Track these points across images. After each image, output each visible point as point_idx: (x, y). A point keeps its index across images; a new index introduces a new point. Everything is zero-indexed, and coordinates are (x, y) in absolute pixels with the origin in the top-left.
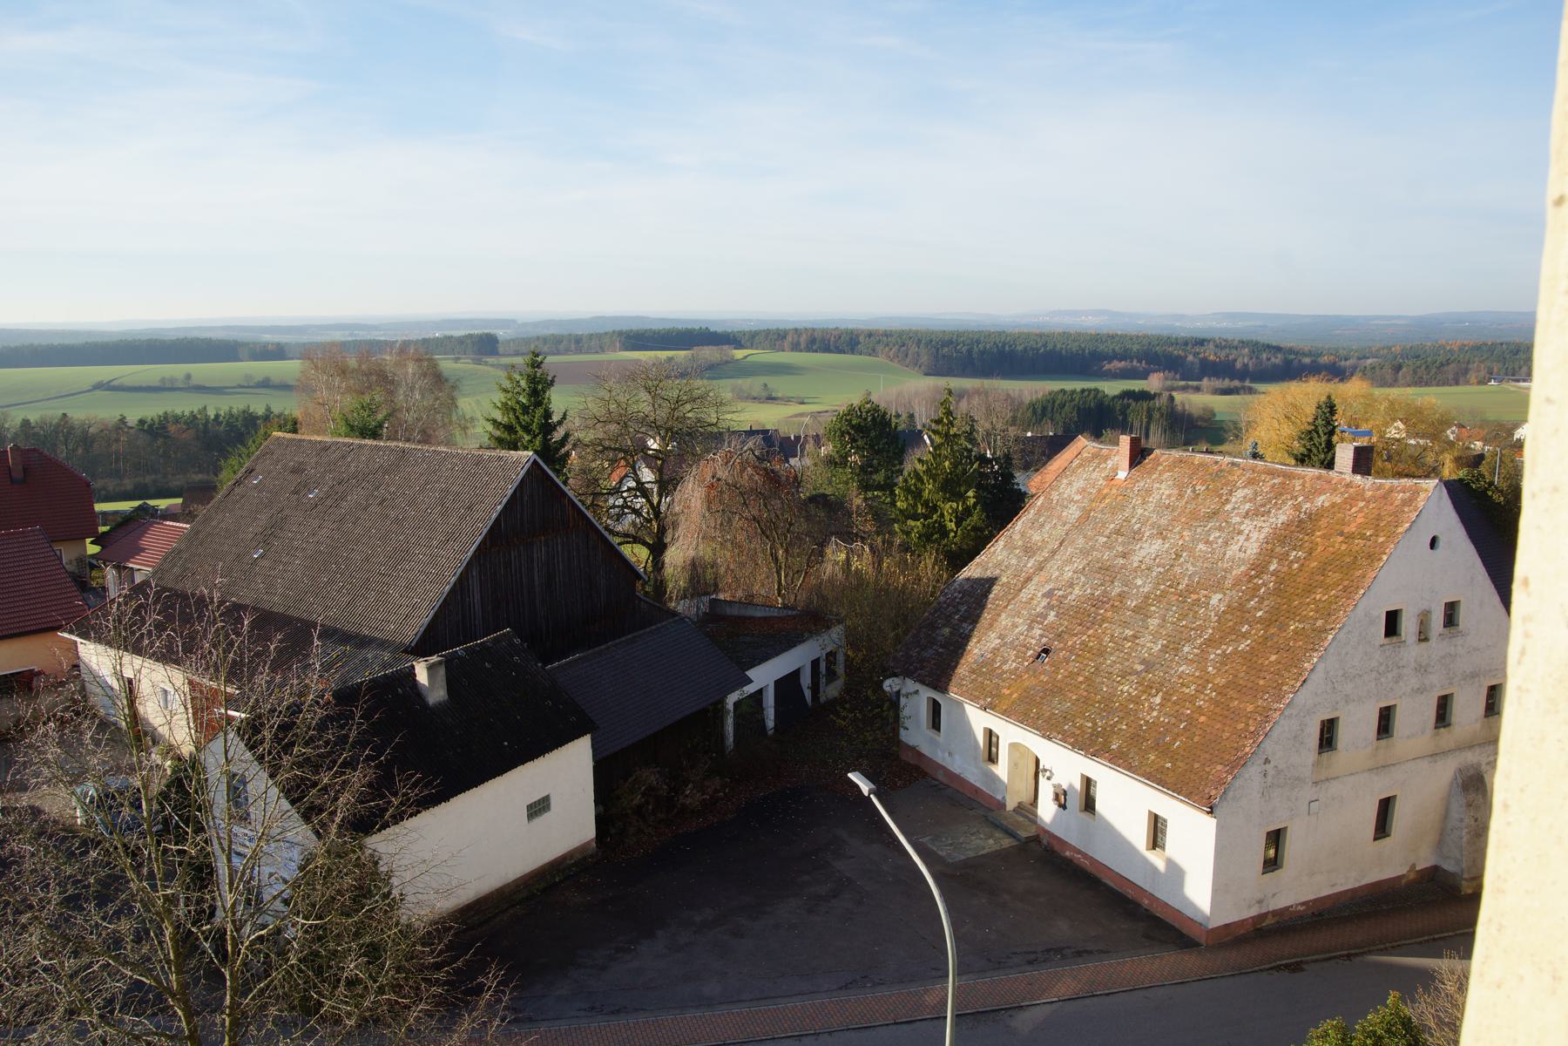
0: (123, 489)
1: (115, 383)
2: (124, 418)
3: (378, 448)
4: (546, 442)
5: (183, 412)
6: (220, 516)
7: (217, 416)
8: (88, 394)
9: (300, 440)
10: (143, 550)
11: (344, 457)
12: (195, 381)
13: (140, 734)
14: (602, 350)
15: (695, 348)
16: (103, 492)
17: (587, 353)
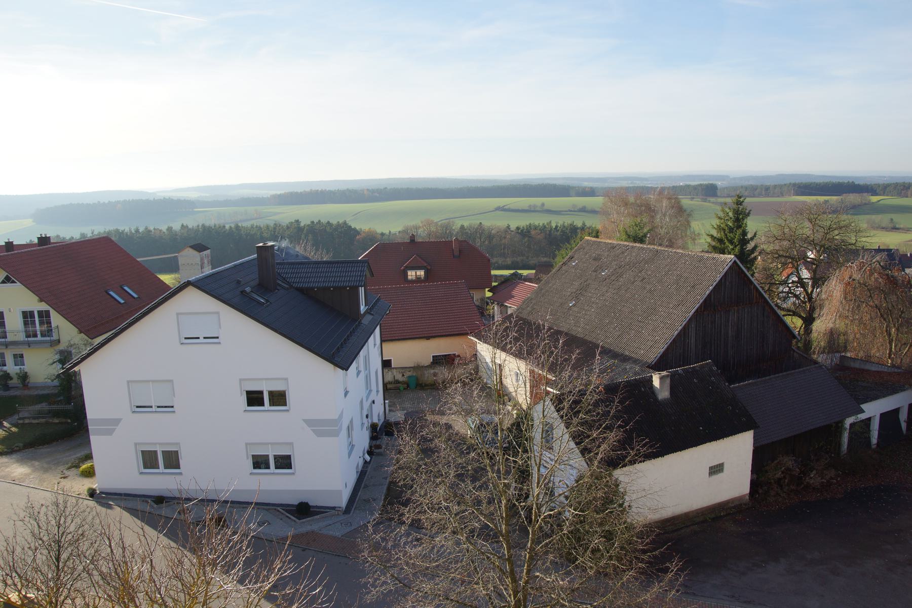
2: (509, 226)
7: (557, 227)
11: (623, 253)
12: (546, 207)
15: (844, 195)
17: (772, 197)
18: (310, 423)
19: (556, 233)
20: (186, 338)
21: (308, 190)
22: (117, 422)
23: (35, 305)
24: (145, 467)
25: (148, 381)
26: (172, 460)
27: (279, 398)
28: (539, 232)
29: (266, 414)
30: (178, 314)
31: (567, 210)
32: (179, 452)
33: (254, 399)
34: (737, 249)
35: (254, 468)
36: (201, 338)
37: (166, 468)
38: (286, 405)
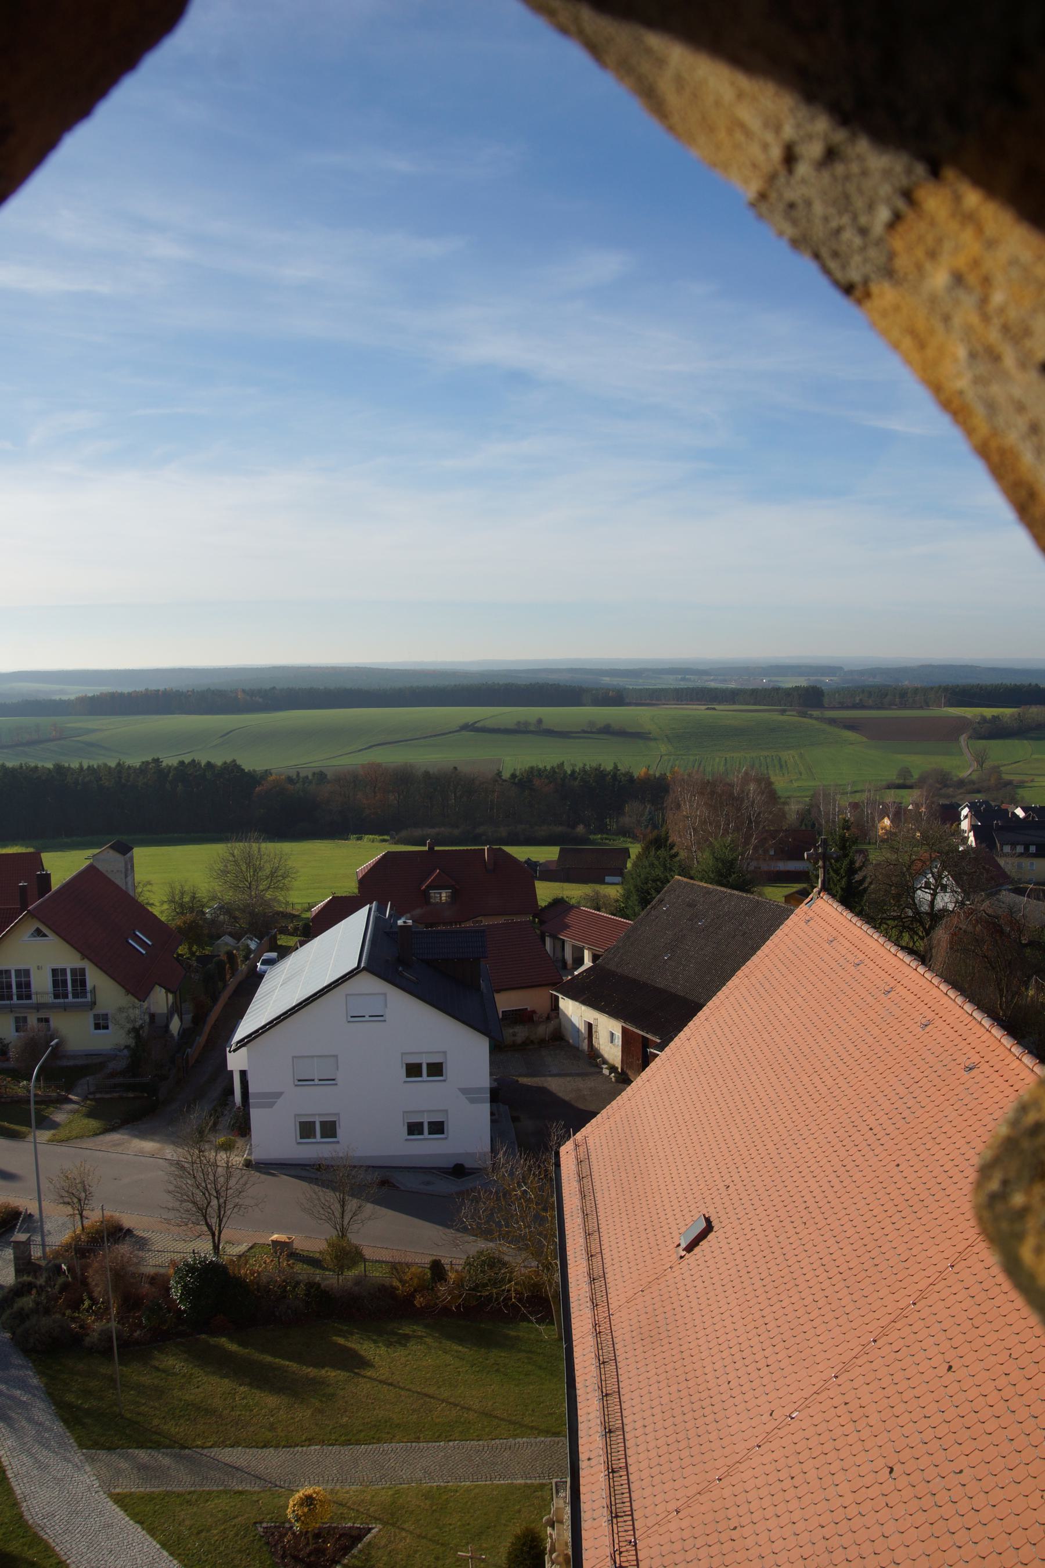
2: (501, 772)
3: (742, 898)
4: (849, 882)
5: (545, 767)
7: (573, 772)
8: (456, 734)
10: (569, 927)
11: (720, 900)
13: (594, 1056)
14: (927, 705)
15: (1023, 707)
16: (484, 838)
17: (911, 708)
20: (352, 1017)
21: (140, 688)
22: (278, 1095)
23: (68, 959)
25: (313, 1057)
26: (330, 1129)
27: (436, 1070)
30: (347, 995)
31: (579, 730)
32: (337, 1123)
33: (413, 1070)
34: (844, 882)
35: (409, 1134)
36: (367, 1017)
37: (322, 1137)
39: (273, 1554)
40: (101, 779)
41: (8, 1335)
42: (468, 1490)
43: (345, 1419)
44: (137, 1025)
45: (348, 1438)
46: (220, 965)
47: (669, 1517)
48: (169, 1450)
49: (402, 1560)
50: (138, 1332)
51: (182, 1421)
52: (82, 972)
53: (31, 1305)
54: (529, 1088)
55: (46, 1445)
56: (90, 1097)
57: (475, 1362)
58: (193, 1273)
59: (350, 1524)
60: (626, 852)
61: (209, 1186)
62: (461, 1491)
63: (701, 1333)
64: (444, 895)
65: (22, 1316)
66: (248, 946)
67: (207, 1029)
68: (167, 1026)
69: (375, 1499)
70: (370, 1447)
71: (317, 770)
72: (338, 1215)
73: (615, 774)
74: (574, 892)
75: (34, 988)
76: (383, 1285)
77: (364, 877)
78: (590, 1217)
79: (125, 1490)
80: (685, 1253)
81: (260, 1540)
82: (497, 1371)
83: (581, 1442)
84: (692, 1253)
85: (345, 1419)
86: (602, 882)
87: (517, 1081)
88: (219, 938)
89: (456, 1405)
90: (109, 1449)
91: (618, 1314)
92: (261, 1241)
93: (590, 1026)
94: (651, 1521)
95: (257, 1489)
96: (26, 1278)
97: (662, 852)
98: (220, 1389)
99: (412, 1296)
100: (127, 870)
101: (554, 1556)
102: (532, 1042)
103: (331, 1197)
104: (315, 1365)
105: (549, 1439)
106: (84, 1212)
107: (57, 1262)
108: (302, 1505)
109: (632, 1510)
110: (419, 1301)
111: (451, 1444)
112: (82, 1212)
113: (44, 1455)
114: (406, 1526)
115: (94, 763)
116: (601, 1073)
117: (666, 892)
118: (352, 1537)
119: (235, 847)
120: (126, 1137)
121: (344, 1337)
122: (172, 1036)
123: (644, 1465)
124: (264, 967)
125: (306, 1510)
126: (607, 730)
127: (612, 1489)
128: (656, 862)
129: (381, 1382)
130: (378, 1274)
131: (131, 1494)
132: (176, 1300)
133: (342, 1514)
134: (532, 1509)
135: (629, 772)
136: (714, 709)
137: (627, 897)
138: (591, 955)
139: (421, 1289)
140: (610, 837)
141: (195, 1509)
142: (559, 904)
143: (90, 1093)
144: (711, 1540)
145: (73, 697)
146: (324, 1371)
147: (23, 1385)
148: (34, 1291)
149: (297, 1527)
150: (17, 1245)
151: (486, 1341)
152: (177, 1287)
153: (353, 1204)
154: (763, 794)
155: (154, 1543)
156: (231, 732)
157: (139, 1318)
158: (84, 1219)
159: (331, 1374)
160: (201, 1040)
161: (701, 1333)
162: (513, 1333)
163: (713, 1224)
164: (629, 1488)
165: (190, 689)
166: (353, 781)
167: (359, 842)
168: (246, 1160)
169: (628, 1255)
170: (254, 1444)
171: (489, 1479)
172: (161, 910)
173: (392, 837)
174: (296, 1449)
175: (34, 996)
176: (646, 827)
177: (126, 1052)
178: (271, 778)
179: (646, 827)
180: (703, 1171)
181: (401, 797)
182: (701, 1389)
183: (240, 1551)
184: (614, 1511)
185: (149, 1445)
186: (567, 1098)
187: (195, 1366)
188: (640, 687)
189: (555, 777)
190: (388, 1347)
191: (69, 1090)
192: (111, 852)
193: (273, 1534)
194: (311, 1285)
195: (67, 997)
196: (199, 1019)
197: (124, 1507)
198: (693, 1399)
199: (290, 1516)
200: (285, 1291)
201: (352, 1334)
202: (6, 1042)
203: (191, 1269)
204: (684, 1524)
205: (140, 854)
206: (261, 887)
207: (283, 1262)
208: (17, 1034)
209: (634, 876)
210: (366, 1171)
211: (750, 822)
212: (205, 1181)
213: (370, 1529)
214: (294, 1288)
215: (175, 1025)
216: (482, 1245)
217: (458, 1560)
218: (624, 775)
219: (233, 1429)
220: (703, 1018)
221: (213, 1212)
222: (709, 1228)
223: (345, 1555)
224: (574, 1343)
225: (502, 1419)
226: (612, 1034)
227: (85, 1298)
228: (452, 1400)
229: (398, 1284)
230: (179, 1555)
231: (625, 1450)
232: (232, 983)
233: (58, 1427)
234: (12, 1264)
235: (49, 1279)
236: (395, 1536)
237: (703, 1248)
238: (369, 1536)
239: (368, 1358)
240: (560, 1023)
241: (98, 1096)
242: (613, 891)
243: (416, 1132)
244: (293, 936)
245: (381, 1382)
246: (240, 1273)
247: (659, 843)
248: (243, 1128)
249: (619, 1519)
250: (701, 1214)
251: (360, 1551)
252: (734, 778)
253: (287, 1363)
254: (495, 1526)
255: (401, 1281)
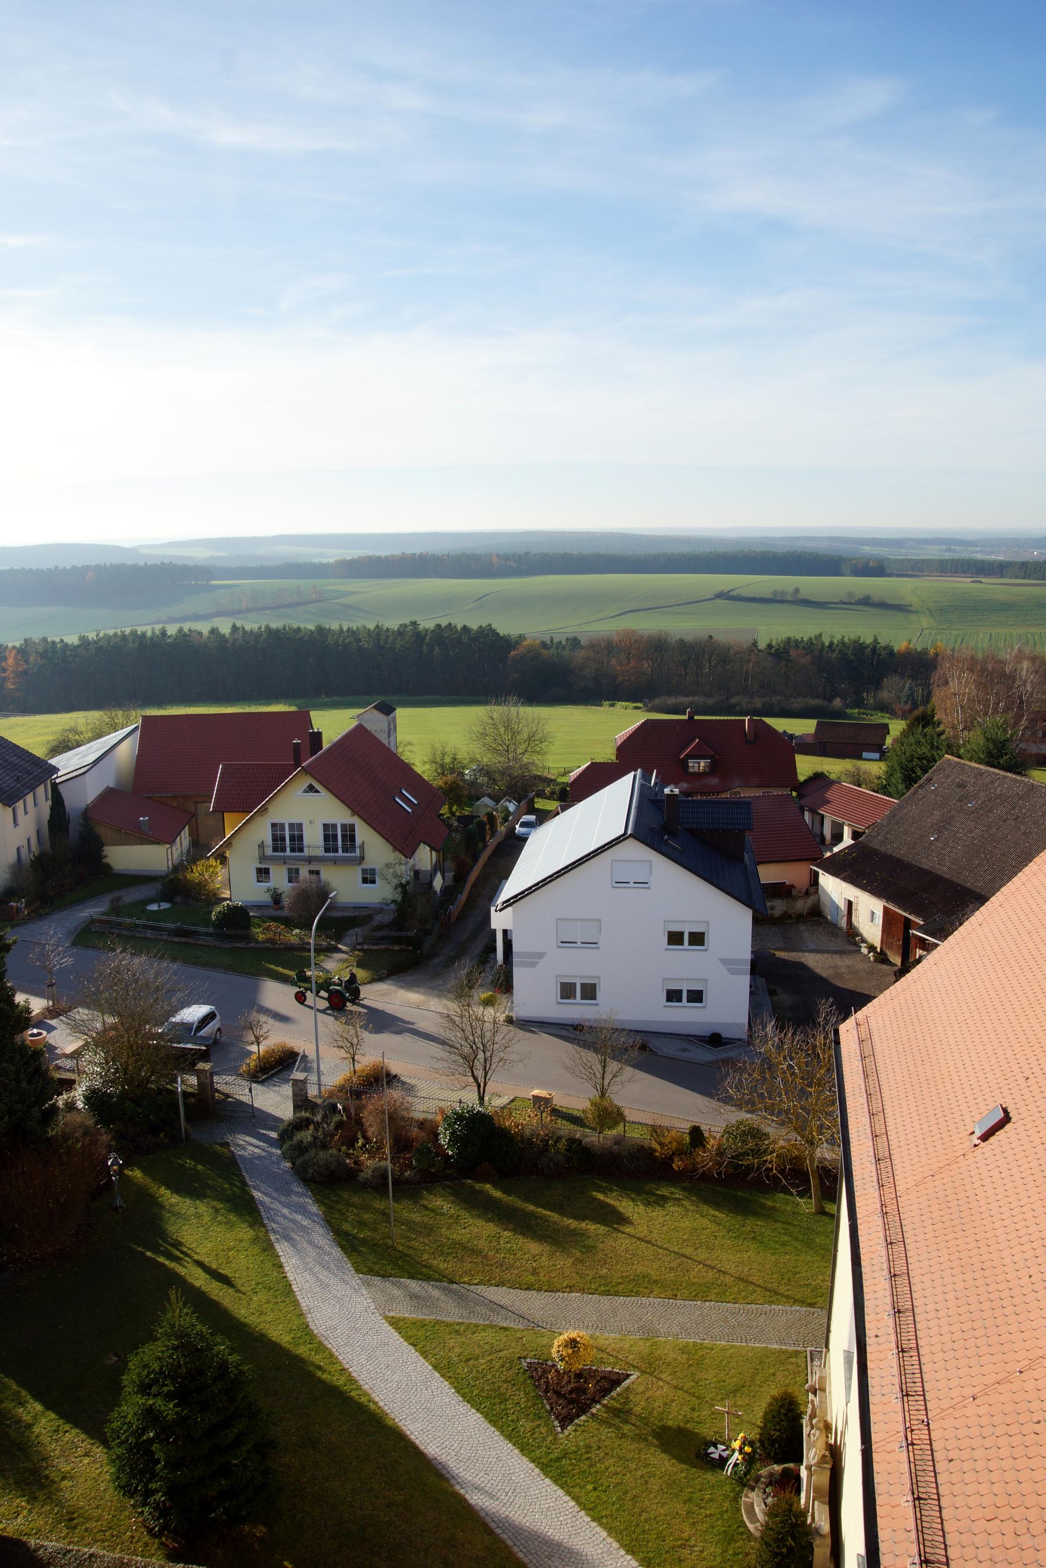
0: (753, 706)
1: (733, 593)
2: (756, 642)
6: (909, 808)
7: (831, 644)
9: (964, 764)
10: (829, 802)
11: (992, 782)
12: (802, 595)
13: (852, 935)
16: (738, 708)
18: (724, 961)
19: (830, 655)
21: (397, 552)
22: (541, 955)
23: (339, 815)
24: (562, 998)
26: (590, 992)
27: (697, 939)
28: (804, 652)
29: (686, 953)
33: (675, 938)
35: (667, 1001)
36: (632, 883)
37: (582, 998)
38: (703, 945)
39: (537, 1387)
40: (360, 641)
41: (288, 1165)
42: (724, 1349)
43: (605, 1271)
44: (404, 881)
45: (608, 1288)
46: (481, 825)
47: (965, 1402)
48: (438, 1284)
49: (659, 1407)
50: (409, 1173)
51: (449, 1258)
52: (352, 827)
53: (309, 1139)
54: (785, 962)
55: (325, 1266)
56: (358, 947)
57: (732, 1228)
58: (461, 1122)
59: (609, 1369)
60: (885, 729)
61: (476, 1039)
62: (717, 1350)
63: (998, 1224)
64: (702, 764)
65: (301, 1149)
66: (507, 808)
67: (468, 887)
68: (431, 883)
69: (634, 1348)
70: (629, 1299)
71: (570, 636)
72: (599, 1076)
73: (874, 647)
74: (833, 767)
75: (306, 841)
76: (642, 1147)
77: (622, 744)
78: (873, 1097)
79: (399, 1315)
80: (979, 1141)
81: (524, 1373)
82: (754, 1238)
83: (867, 1318)
84: (987, 1142)
85: (605, 1271)
86: (859, 757)
87: (774, 954)
88: (478, 799)
89: (713, 1268)
90: (383, 1276)
91: (906, 1197)
92: (522, 1095)
93: (850, 904)
94: (945, 1404)
95: (520, 1327)
96: (304, 1114)
97: (929, 730)
98: (484, 1232)
99: (671, 1158)
100: (389, 730)
101: (814, 1421)
102: (790, 916)
103: (592, 1058)
104: (576, 1218)
105: (805, 1309)
106: (356, 1057)
107: (333, 1101)
108: (566, 1346)
109: (923, 1390)
110: (677, 1164)
111: (707, 1304)
112: (354, 1056)
113: (324, 1275)
114: (663, 1376)
115: (354, 626)
116: (859, 951)
117: (935, 771)
118: (611, 1380)
119: (495, 711)
120: (392, 988)
121: (604, 1193)
122: (435, 892)
123: (937, 1348)
124: (523, 830)
125: (570, 1351)
126: (866, 602)
127: (902, 1368)
128: (923, 740)
129: (639, 1239)
130: (636, 1134)
131: (404, 1319)
132: (444, 1146)
133: (601, 1358)
134: (786, 1373)
135: (889, 646)
136: (981, 582)
137: (890, 774)
138: (851, 832)
139: (680, 1152)
140: (867, 712)
141: (463, 1339)
142: (819, 779)
143: (359, 944)
144: (1011, 1430)
145: (332, 560)
146: (584, 1224)
147: (303, 1210)
148: (311, 1127)
149: (561, 1366)
150: (296, 1082)
151: (743, 1208)
152: (445, 1134)
153: (613, 1066)
154: (1037, 672)
155: (427, 1364)
156: (485, 596)
157: (410, 1159)
158: (356, 1063)
159: (591, 1227)
160: (463, 897)
161: (998, 1224)
162: (769, 1203)
163: (1011, 1115)
164: (921, 1369)
165: (446, 553)
166: (608, 647)
167: (612, 708)
168: (507, 1016)
169: (916, 1139)
170: (517, 1286)
171: (744, 1340)
172: (423, 768)
173: (645, 705)
174: (558, 1294)
175: (306, 849)
176: (906, 703)
177: (393, 906)
178: (525, 643)
179: (906, 703)
180: (999, 1060)
181: (655, 665)
182: (999, 1279)
183: (505, 1381)
184: (904, 1389)
185: (419, 1276)
186: (824, 975)
187: (462, 1208)
188: (902, 558)
189: (813, 649)
190: (646, 1206)
191: (339, 940)
192: (375, 712)
193: (536, 1369)
194: (572, 1141)
195: (337, 852)
196: (460, 878)
197: (399, 1330)
198: (991, 1289)
199: (555, 1355)
200: (547, 1145)
201: (611, 1191)
202: (279, 891)
203: (460, 1117)
204: (981, 1411)
205: (402, 714)
206: (519, 751)
207: (546, 1118)
208: (290, 884)
209: (899, 753)
210: (628, 1034)
211: (1022, 702)
212: (473, 1035)
213: (628, 1376)
214: (556, 1142)
215: (438, 883)
216: (744, 1116)
217: (713, 1413)
218: (884, 648)
219: (498, 1270)
220: (997, 904)
221: (478, 1065)
222: (1006, 1119)
223: (604, 1396)
224: (859, 1221)
225: (758, 1286)
226: (873, 913)
227: (359, 1136)
228: (708, 1262)
229: (658, 1148)
230: (450, 1377)
231: (916, 1332)
232: (492, 843)
233: (337, 1252)
234: (291, 1101)
235: (325, 1116)
236: (653, 1384)
237: (1000, 1138)
238: (627, 1382)
239: (627, 1215)
240: (819, 900)
241: (366, 947)
242: (874, 768)
243: (675, 999)
244: (549, 799)
245: (639, 1239)
246: (504, 1124)
247: (926, 720)
248: (505, 984)
249: (910, 1398)
250: (998, 1103)
251: (619, 1394)
252: (1005, 655)
253: (549, 1213)
254: (750, 1386)
255: (660, 1143)
